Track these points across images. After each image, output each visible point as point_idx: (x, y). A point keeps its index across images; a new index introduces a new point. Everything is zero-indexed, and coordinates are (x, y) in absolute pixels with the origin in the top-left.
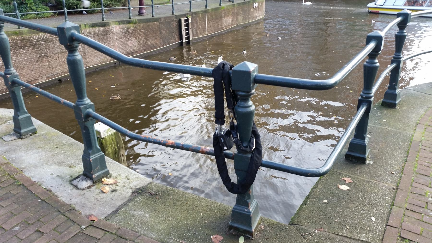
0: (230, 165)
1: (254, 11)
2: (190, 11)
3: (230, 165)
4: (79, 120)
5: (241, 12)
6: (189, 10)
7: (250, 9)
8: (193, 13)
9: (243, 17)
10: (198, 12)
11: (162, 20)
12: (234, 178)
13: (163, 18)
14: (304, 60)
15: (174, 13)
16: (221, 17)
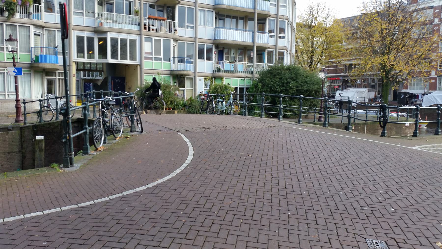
0: (382, 123)
1: (406, 129)
2: (354, 122)
3: (382, 123)
4: (341, 53)
5: (394, 128)
6: (353, 121)
7: (403, 127)
8: (356, 123)
9: (396, 132)
10: (360, 123)
11: (334, 125)
12: (382, 126)
13: (335, 124)
14: (409, 58)
15: (343, 122)
16: (377, 130)
